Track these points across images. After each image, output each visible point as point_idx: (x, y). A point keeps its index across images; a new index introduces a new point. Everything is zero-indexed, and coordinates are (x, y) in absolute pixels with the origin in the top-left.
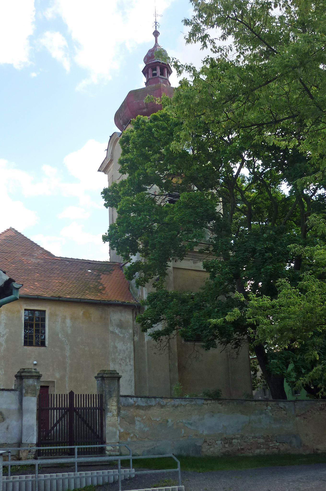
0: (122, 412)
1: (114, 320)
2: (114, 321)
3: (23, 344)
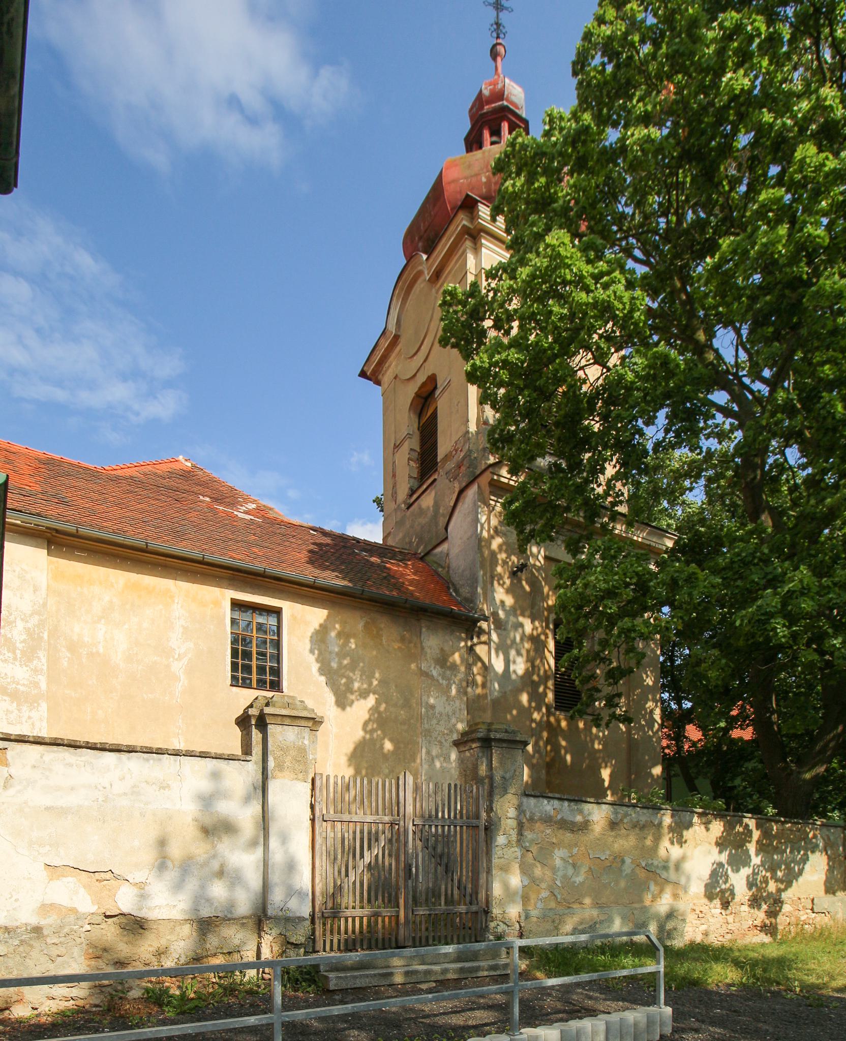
0: (528, 835)
1: (430, 648)
2: (429, 651)
3: (229, 681)
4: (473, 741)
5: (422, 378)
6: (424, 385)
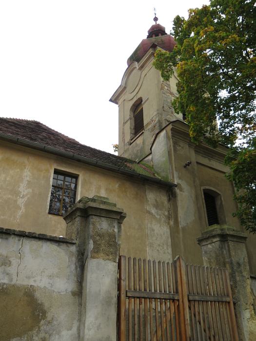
3: (47, 211)
4: (214, 237)
5: (135, 100)
6: (137, 101)
